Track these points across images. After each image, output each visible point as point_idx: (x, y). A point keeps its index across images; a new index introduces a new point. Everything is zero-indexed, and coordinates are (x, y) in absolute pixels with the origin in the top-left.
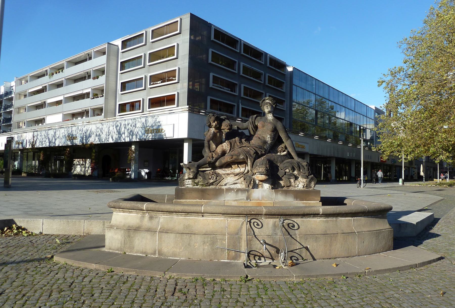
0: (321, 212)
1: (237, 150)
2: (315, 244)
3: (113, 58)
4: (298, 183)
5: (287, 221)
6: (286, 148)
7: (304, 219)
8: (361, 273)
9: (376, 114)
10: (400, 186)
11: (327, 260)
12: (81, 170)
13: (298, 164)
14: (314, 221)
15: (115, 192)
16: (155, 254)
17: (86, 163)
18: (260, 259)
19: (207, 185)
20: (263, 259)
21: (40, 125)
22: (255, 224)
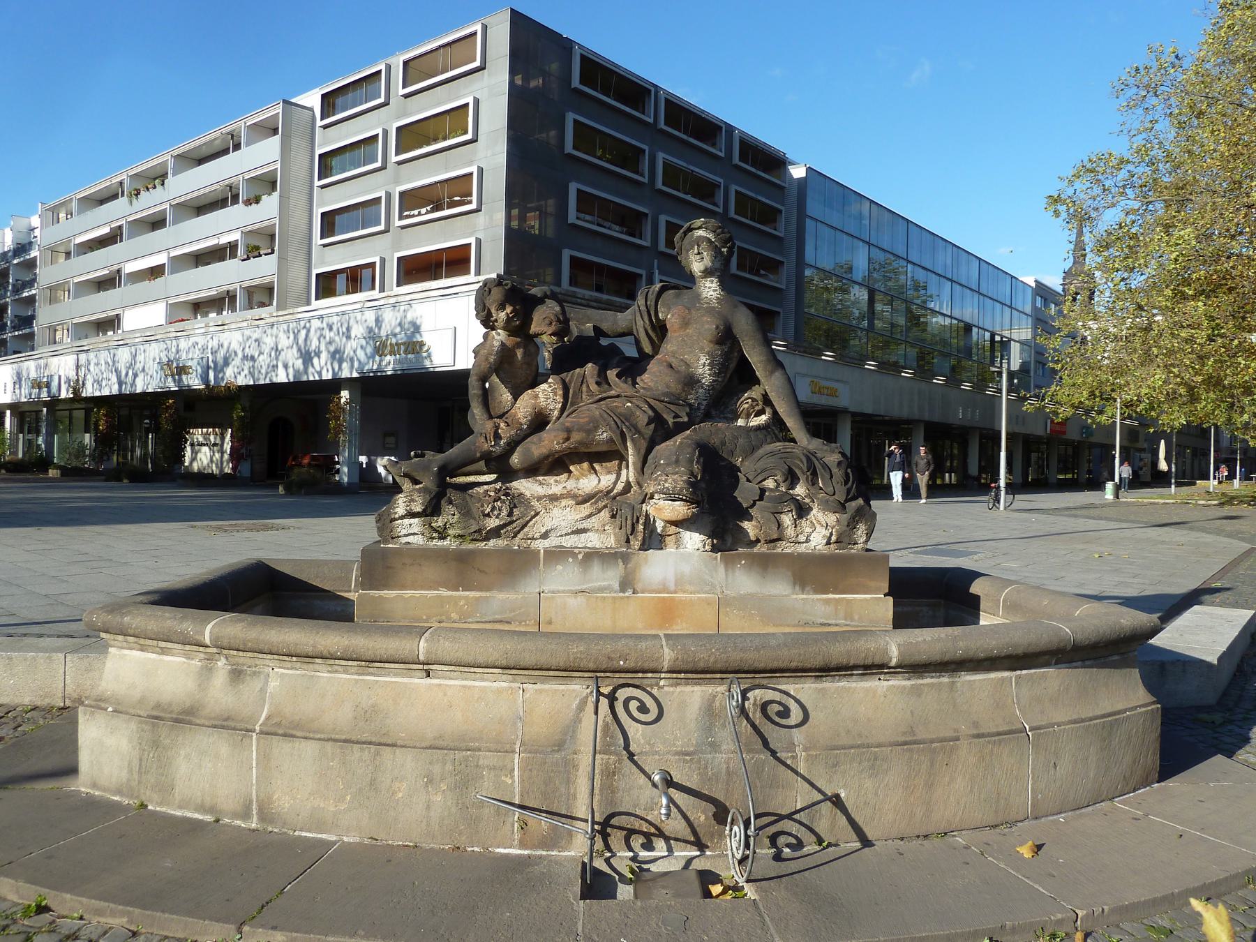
0: (894, 656)
1: (588, 409)
2: (868, 783)
3: (299, 144)
4: (808, 530)
5: (757, 695)
6: (767, 401)
7: (827, 685)
8: (1060, 922)
9: (1039, 299)
10: (1110, 505)
11: (915, 843)
12: (212, 461)
13: (810, 458)
14: (867, 690)
15: (272, 528)
16: (246, 815)
17: (223, 439)
18: (648, 846)
19: (476, 536)
20: (660, 844)
21: (110, 333)
22: (633, 705)
